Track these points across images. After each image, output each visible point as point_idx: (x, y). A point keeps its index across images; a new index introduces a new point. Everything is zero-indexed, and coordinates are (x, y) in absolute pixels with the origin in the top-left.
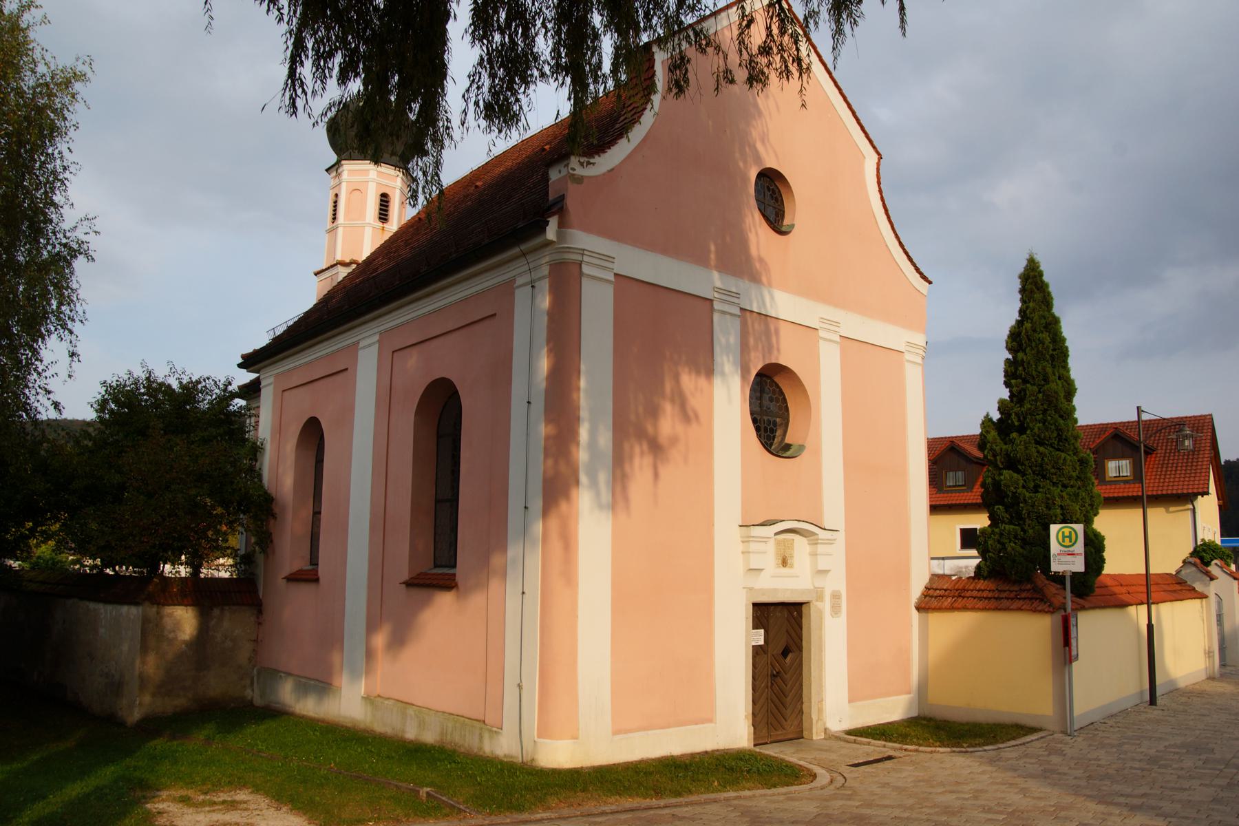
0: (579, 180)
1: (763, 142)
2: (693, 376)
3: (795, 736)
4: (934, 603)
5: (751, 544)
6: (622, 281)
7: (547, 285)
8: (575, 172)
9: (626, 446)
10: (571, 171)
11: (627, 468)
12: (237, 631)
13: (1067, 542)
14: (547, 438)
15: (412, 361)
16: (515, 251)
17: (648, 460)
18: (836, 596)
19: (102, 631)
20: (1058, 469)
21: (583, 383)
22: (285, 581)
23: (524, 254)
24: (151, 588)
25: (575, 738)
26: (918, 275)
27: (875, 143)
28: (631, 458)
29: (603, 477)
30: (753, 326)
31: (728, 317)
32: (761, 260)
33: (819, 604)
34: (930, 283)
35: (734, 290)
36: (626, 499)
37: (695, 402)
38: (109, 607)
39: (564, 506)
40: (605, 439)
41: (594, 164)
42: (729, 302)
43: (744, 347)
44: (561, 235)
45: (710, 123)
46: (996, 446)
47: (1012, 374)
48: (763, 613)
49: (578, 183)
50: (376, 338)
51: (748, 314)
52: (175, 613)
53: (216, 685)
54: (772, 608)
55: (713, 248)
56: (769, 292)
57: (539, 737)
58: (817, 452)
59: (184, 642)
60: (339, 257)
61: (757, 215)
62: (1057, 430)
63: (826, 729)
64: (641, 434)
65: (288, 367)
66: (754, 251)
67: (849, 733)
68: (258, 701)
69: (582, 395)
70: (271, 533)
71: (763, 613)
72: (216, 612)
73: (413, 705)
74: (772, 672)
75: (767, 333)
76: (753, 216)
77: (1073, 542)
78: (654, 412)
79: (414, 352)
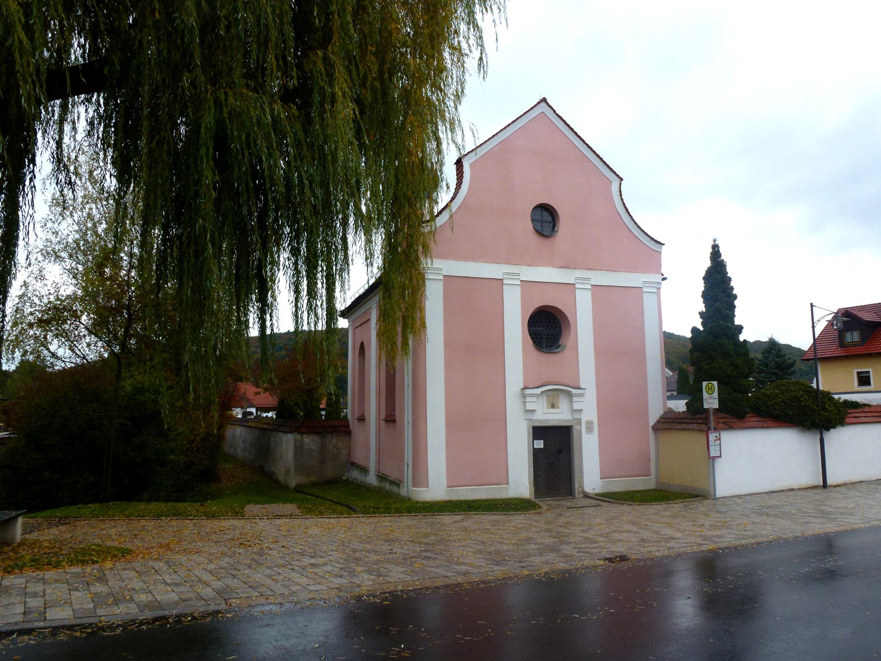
4: (666, 426)
6: (525, 284)
13: (710, 392)
18: (589, 424)
22: (357, 420)
27: (617, 173)
46: (89, 345)
48: (539, 432)
71: (539, 432)
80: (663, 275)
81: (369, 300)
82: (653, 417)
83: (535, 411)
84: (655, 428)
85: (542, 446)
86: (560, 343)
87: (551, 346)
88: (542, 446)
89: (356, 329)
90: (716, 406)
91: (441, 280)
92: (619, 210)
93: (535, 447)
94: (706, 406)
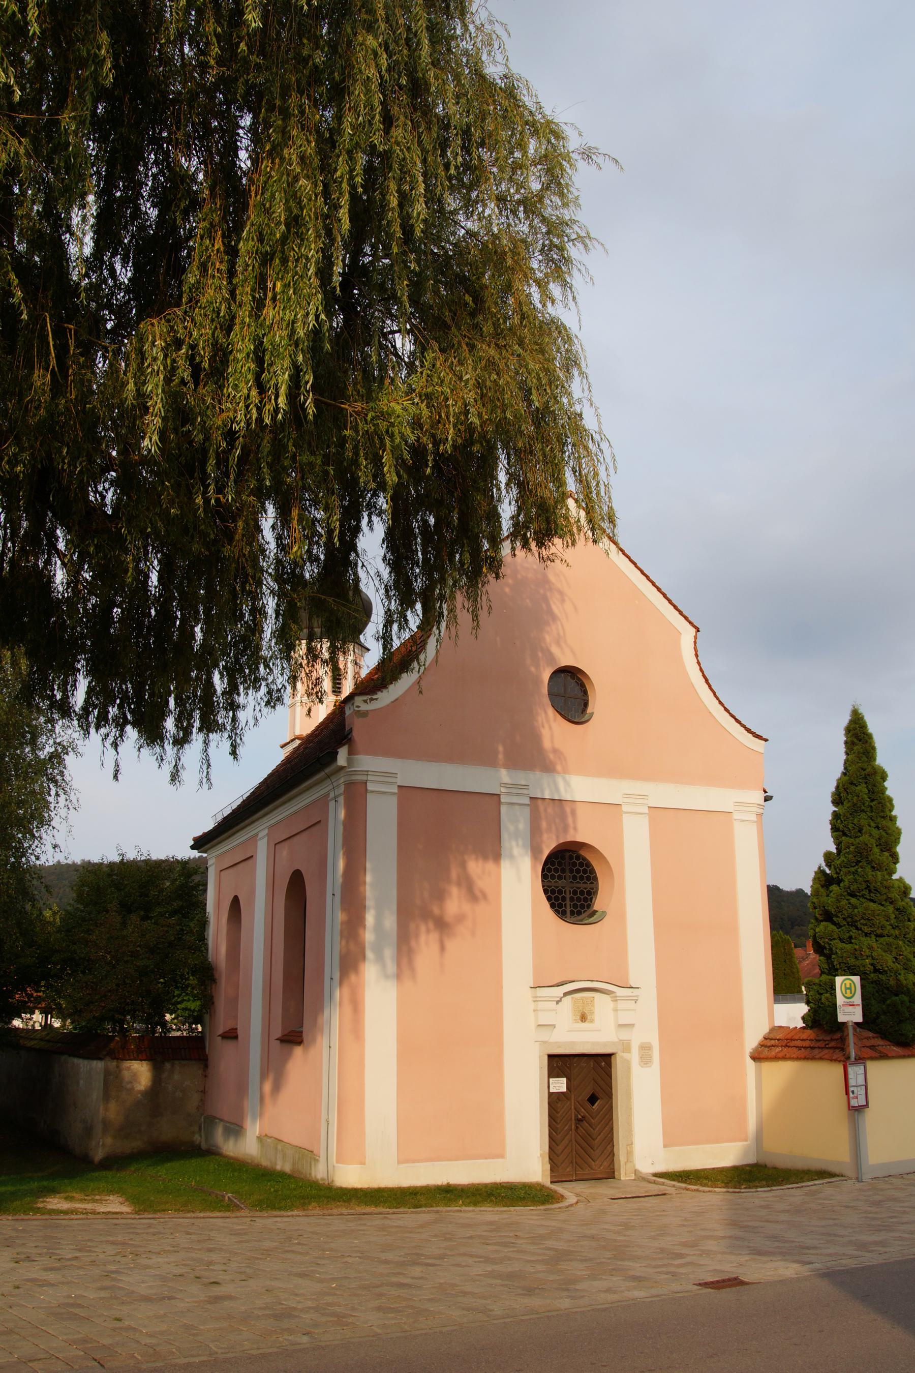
0: (365, 714)
1: (558, 644)
2: (480, 862)
3: (604, 1176)
4: (766, 1052)
5: (540, 1003)
7: (343, 801)
8: (360, 709)
9: (412, 926)
10: (357, 709)
11: (413, 943)
12: (186, 1083)
14: (342, 923)
15: (284, 852)
16: (321, 775)
17: (434, 936)
18: (645, 1048)
19: (81, 1082)
20: (868, 919)
21: (369, 878)
23: (328, 776)
24: (112, 1045)
25: (363, 1163)
26: (750, 736)
27: (690, 619)
28: (417, 936)
29: (389, 953)
30: (545, 810)
31: (517, 807)
32: (555, 751)
33: (625, 1055)
34: (766, 740)
35: (523, 783)
36: (412, 969)
37: (481, 884)
38: (86, 1062)
39: (353, 978)
40: (390, 922)
41: (376, 699)
42: (517, 795)
43: (535, 830)
44: (350, 761)
45: (498, 639)
47: (838, 827)
49: (364, 717)
50: (266, 831)
51: (540, 802)
52: (132, 1067)
53: (167, 1130)
54: (576, 1059)
55: (501, 748)
56: (564, 779)
57: (337, 1163)
58: (622, 917)
59: (140, 1092)
60: (298, 733)
61: (551, 711)
62: (865, 881)
63: (636, 1171)
64: (426, 915)
65: (241, 840)
66: (547, 744)
67: (656, 1175)
68: (204, 1146)
69: (368, 888)
70: (213, 997)
72: (168, 1066)
73: (282, 1141)
74: (576, 1116)
75: (563, 817)
76: (546, 713)
77: (853, 992)
78: (440, 896)
79: (286, 844)
80: (765, 792)
81: (253, 822)
82: (753, 1037)
83: (633, 1025)
84: (756, 1057)
85: (564, 1089)
86: (595, 908)
87: (579, 913)
88: (564, 1089)
89: (222, 873)
90: (859, 1018)
91: (393, 793)
92: (694, 681)
93: (552, 1090)
94: (841, 1018)
